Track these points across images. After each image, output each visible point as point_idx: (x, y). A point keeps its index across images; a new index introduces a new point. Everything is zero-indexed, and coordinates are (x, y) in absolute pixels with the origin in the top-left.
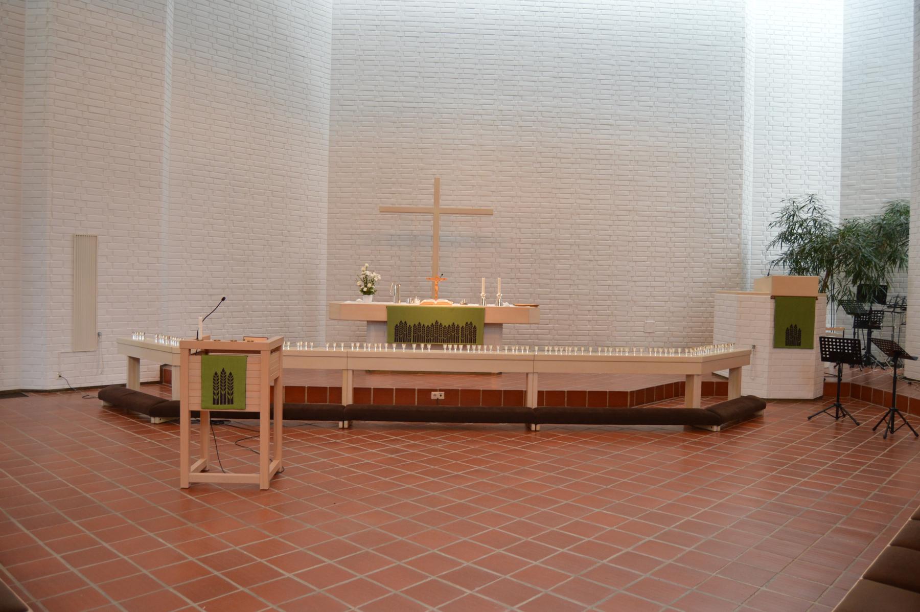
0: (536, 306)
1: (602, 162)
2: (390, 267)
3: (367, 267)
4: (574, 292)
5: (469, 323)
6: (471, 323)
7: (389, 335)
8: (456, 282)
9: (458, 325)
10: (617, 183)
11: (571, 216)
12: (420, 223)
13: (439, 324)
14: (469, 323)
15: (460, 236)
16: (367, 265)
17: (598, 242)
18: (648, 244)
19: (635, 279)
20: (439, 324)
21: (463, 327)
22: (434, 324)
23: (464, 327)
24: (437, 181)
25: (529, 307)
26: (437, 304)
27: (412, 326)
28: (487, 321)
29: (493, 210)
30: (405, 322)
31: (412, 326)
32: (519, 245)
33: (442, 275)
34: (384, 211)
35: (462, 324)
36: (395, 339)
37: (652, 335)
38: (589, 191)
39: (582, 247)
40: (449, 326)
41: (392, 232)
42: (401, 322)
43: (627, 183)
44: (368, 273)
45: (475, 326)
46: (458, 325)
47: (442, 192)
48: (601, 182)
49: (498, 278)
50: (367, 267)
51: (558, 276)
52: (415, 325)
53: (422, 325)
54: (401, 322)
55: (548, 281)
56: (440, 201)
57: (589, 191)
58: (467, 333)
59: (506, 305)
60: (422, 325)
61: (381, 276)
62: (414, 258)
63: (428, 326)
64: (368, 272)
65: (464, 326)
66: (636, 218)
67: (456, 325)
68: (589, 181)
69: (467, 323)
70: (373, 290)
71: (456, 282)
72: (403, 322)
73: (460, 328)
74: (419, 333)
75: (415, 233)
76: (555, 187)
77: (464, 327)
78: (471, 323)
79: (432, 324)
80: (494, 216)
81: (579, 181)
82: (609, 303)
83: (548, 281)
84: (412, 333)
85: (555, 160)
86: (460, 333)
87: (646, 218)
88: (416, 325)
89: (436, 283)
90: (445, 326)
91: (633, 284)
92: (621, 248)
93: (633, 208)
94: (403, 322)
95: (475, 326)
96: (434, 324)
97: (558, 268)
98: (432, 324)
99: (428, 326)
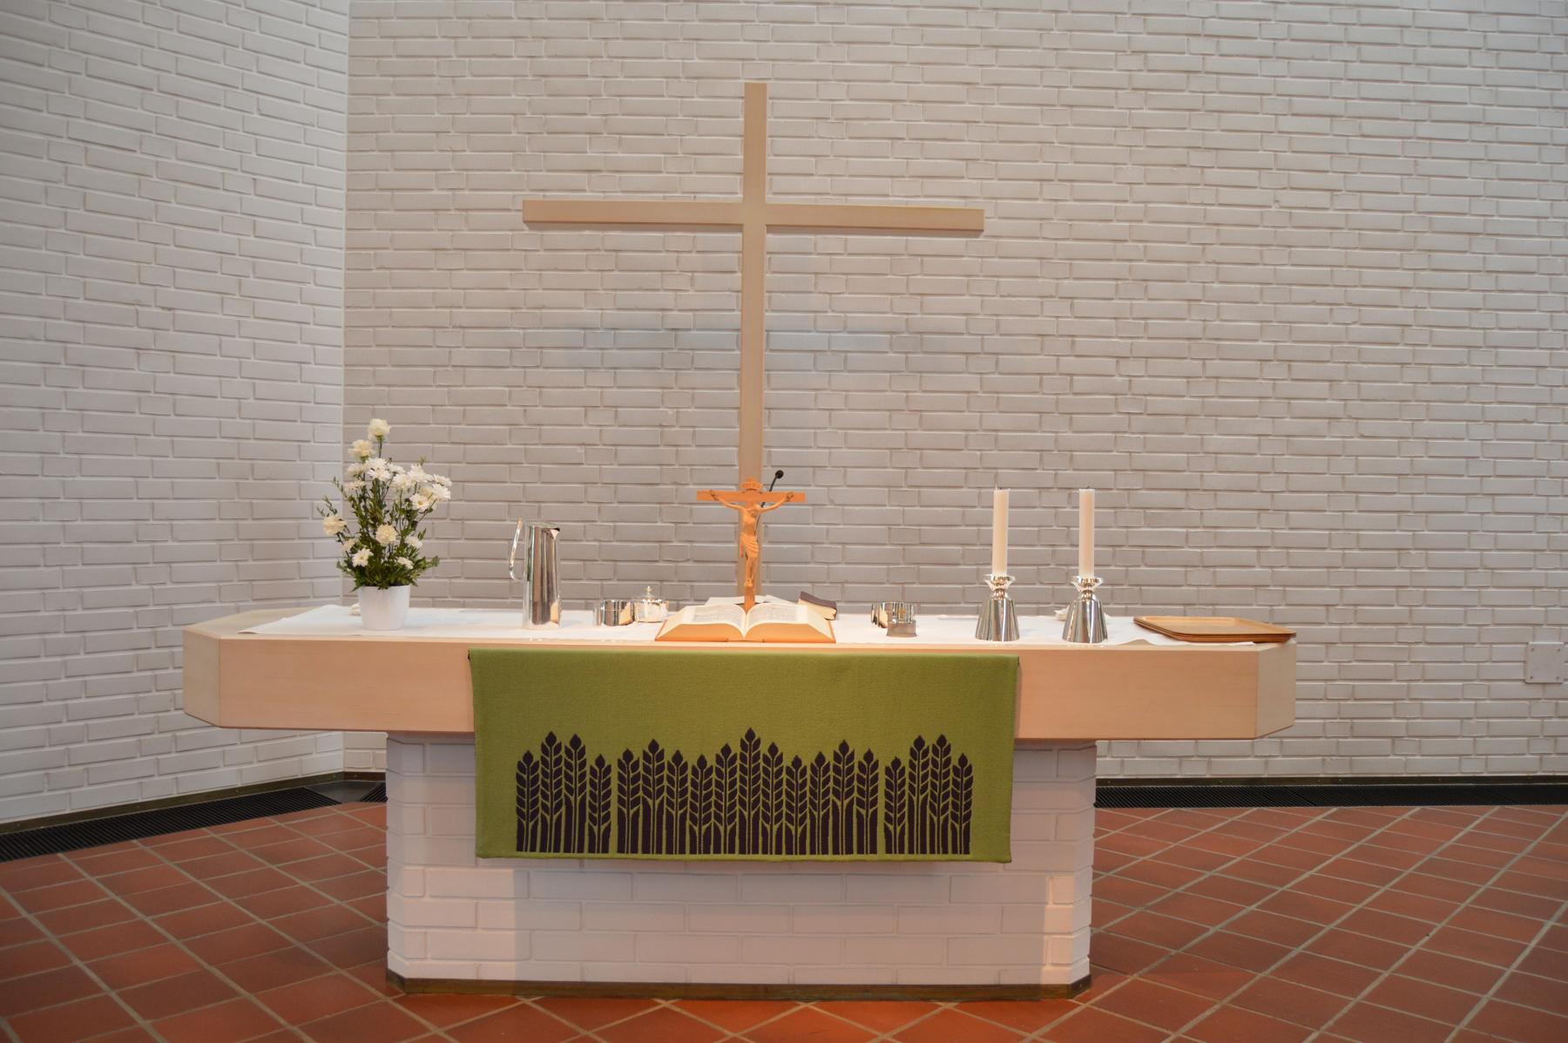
0: (1282, 638)
1: (1369, 52)
2: (580, 450)
3: (380, 438)
4: (1273, 536)
5: (930, 741)
6: (942, 740)
7: (484, 807)
8: (832, 502)
9: (869, 756)
10: (1426, 129)
11: (1261, 253)
12: (692, 279)
13: (764, 749)
14: (930, 741)
15: (845, 330)
16: (380, 425)
17: (1360, 351)
18: (1541, 356)
19: (1494, 485)
20: (764, 749)
21: (896, 763)
22: (736, 749)
23: (905, 763)
24: (755, 97)
25: (1248, 646)
26: (757, 633)
27: (612, 760)
28: (1029, 728)
29: (981, 212)
30: (576, 741)
31: (612, 760)
32: (1070, 363)
33: (779, 475)
34: (542, 220)
35: (891, 747)
36: (520, 830)
37: (1552, 691)
38: (1323, 161)
39: (1300, 369)
40: (820, 758)
41: (589, 314)
42: (551, 738)
43: (1461, 131)
44: (379, 468)
45: (963, 760)
46: (869, 756)
47: (772, 162)
48: (1369, 126)
49: (997, 492)
50: (380, 438)
51: (1214, 479)
52: (628, 755)
53: (668, 758)
54: (551, 738)
55: (1178, 498)
56: (770, 158)
57: (1323, 161)
58: (918, 799)
59: (1122, 632)
60: (668, 758)
61: (458, 483)
62: (670, 412)
63: (702, 761)
64: (379, 463)
65: (905, 760)
66: (1497, 261)
67: (859, 757)
68: (1323, 124)
69: (919, 742)
70: (406, 562)
71: (832, 502)
72: (564, 740)
73: (881, 771)
74: (653, 803)
75: (676, 318)
76: (1200, 144)
77: (905, 763)
78: (942, 740)
79: (726, 750)
80: (984, 233)
81: (1287, 123)
82: (1399, 575)
83: (1178, 498)
84: (614, 798)
85: (1198, 45)
86: (882, 800)
87: (1530, 262)
88: (637, 755)
89: (748, 519)
90: (797, 762)
91: (1484, 504)
92: (1440, 373)
93: (1485, 223)
94: (564, 740)
95: (963, 760)
96: (736, 749)
97: (1211, 449)
98: (726, 750)
99: (702, 761)
